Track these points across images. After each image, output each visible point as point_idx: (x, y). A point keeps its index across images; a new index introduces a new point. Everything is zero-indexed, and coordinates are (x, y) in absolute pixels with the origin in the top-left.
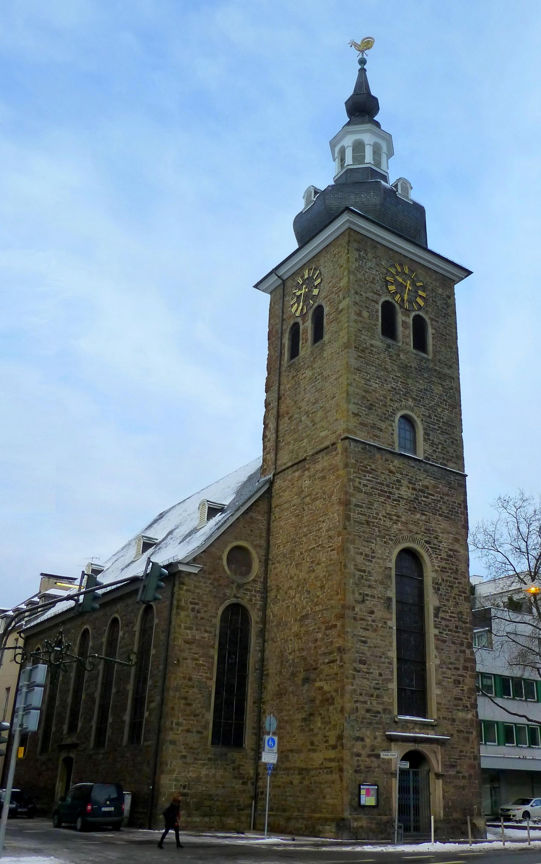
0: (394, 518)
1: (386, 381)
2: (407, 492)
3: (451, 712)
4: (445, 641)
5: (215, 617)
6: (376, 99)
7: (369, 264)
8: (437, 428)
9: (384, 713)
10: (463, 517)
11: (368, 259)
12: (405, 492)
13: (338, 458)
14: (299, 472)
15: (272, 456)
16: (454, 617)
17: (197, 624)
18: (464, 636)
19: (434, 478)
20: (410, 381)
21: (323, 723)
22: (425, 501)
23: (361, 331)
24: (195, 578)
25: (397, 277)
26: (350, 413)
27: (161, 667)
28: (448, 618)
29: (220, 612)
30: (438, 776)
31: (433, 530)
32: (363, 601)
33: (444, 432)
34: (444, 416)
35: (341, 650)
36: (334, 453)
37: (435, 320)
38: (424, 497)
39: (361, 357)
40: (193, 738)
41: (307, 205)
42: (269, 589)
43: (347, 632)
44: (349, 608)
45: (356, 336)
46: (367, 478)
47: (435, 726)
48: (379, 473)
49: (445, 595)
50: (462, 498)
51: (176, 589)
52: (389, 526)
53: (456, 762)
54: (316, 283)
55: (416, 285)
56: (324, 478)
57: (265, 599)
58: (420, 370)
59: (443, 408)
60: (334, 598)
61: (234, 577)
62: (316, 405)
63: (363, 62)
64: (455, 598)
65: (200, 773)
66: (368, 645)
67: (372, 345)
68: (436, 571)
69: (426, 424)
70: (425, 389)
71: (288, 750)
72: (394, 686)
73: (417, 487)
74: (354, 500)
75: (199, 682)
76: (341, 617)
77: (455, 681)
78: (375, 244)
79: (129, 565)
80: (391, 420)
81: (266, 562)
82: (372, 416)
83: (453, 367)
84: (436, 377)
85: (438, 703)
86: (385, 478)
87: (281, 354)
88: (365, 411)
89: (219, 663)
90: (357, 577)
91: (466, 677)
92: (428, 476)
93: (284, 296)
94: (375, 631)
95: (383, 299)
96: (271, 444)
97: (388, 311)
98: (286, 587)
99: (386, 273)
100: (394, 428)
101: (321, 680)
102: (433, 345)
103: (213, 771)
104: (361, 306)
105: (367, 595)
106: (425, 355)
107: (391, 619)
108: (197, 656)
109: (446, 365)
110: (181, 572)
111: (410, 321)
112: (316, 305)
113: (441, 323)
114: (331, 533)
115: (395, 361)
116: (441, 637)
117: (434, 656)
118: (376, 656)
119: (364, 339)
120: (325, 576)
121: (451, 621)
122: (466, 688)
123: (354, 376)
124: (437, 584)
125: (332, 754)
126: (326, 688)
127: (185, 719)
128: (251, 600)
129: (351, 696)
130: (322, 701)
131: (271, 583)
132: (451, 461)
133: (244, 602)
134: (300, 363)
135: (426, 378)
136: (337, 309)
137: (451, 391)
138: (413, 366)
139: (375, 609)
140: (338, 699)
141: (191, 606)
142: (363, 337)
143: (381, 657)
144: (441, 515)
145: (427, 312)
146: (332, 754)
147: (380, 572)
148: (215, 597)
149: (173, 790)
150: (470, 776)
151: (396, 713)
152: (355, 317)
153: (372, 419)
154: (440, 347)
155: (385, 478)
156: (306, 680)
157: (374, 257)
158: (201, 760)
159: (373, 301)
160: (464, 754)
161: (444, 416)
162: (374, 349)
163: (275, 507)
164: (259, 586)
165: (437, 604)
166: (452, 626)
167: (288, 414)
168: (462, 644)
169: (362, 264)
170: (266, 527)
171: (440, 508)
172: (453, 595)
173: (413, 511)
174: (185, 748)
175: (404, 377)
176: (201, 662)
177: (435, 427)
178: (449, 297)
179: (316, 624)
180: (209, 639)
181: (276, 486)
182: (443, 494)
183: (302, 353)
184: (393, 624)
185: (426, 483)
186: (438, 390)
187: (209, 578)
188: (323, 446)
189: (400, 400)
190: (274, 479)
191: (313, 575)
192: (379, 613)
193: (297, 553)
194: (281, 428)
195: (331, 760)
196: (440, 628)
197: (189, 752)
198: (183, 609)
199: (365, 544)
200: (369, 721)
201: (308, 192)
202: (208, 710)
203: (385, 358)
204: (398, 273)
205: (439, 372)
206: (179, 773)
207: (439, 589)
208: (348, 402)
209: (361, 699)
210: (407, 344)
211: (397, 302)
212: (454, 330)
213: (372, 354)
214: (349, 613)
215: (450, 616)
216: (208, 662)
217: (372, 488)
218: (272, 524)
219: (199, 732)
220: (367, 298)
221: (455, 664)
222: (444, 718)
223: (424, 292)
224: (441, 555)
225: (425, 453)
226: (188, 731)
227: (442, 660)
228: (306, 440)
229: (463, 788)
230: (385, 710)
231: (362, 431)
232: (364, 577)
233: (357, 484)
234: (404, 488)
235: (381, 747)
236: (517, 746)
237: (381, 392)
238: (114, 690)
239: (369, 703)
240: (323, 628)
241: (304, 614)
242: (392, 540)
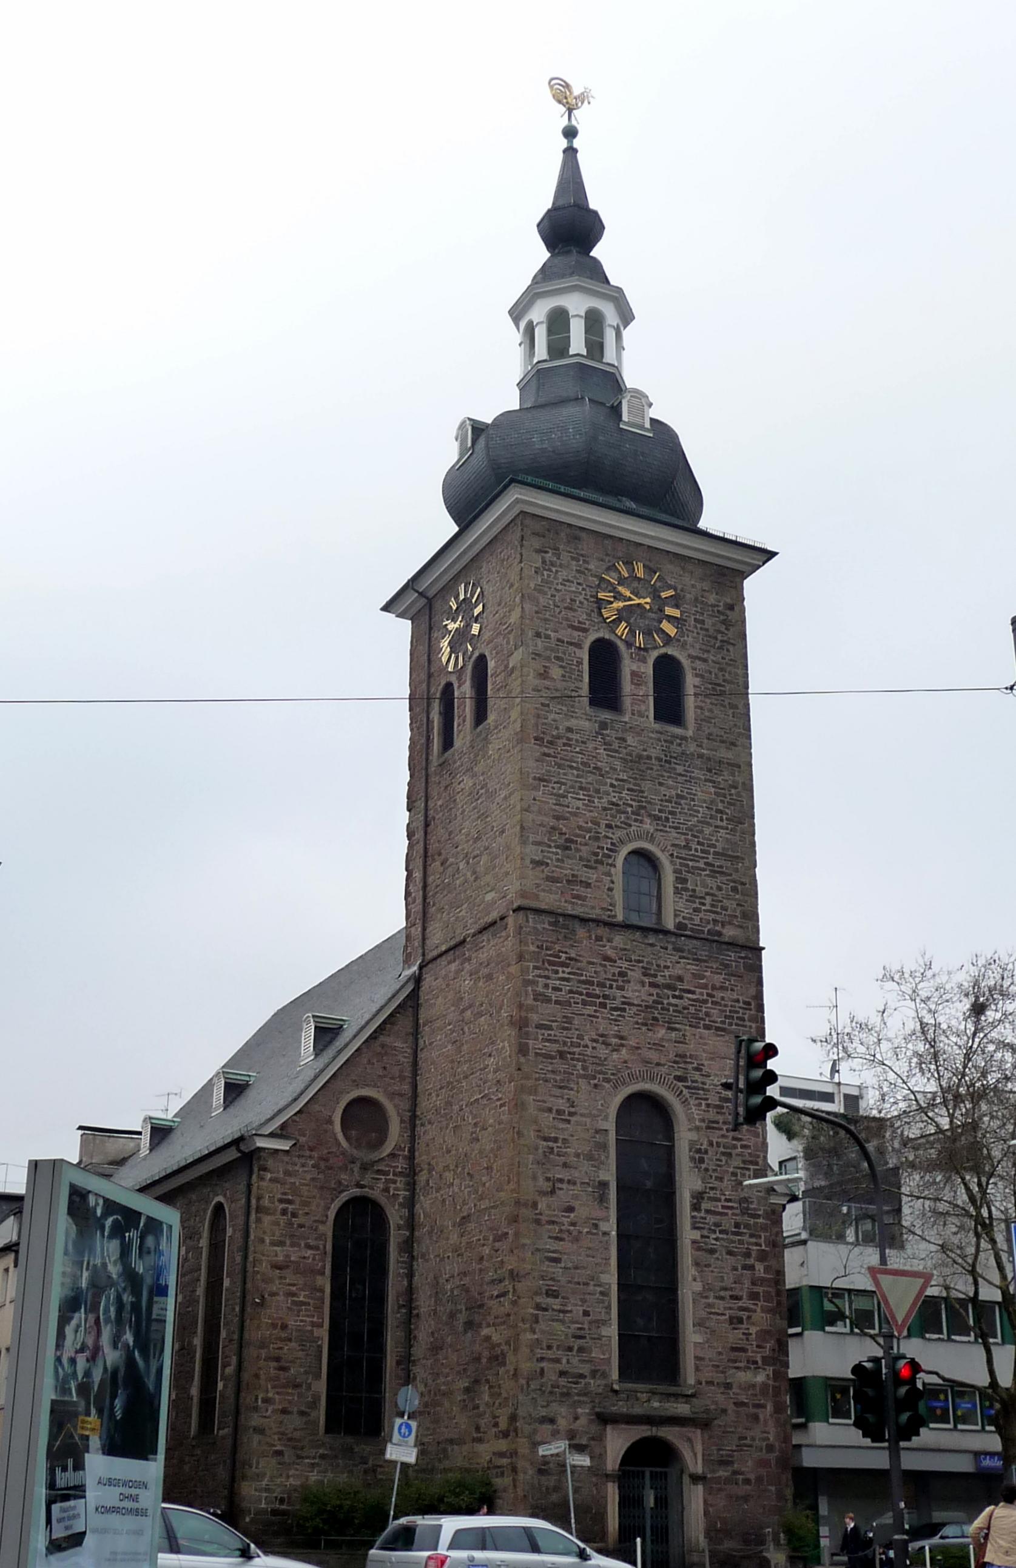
0: (614, 1041)
1: (598, 791)
2: (639, 991)
3: (723, 1372)
4: (712, 1251)
5: (323, 1223)
6: (595, 214)
7: (563, 574)
8: (703, 866)
9: (594, 1377)
10: (754, 1025)
11: (561, 566)
12: (637, 992)
13: (509, 943)
14: (457, 963)
15: (417, 931)
16: (731, 1208)
17: (292, 1236)
18: (753, 1240)
19: (694, 960)
20: (646, 785)
21: (491, 1395)
22: (676, 1006)
23: (548, 705)
24: (286, 1159)
25: (620, 588)
26: (528, 862)
27: (237, 1309)
28: (720, 1210)
29: (332, 1214)
30: (696, 1479)
31: (691, 1056)
32: (553, 1192)
33: (718, 872)
34: (717, 841)
35: (514, 1276)
36: (504, 934)
37: (700, 659)
38: (674, 997)
39: (548, 755)
40: (294, 1422)
41: (461, 456)
42: (418, 1169)
43: (524, 1245)
44: (526, 1205)
45: (538, 716)
46: (561, 975)
47: (693, 1396)
48: (583, 965)
49: (714, 1170)
50: (752, 991)
51: (254, 1177)
52: (603, 1056)
53: (732, 1456)
54: (477, 611)
55: (659, 597)
56: (489, 977)
57: (412, 1186)
58: (669, 762)
59: (716, 827)
60: (506, 1187)
62: (479, 844)
63: (570, 133)
64: (734, 1174)
65: (307, 1478)
66: (563, 1265)
67: (569, 730)
68: (698, 1129)
69: (678, 861)
70: (677, 795)
71: (447, 1440)
72: (612, 1331)
73: (660, 980)
74: (534, 1018)
75: (297, 1331)
76: (514, 1219)
77: (731, 1318)
78: (576, 533)
80: (608, 864)
81: (412, 1121)
82: (570, 862)
83: (739, 743)
84: (701, 769)
85: (697, 1358)
86: (595, 972)
87: (429, 740)
88: (557, 854)
90: (540, 1151)
91: (755, 1311)
92: (680, 958)
93: (431, 629)
94: (576, 1240)
95: (592, 637)
96: (417, 907)
97: (604, 658)
98: (440, 1167)
99: (599, 586)
100: (614, 878)
101: (489, 1326)
102: (696, 707)
103: (330, 1475)
104: (548, 659)
105: (561, 1181)
106: (678, 731)
108: (294, 1288)
109: (722, 742)
110: (260, 1149)
112: (476, 654)
113: (713, 661)
114: (501, 1075)
115: (616, 751)
116: (706, 1244)
117: (690, 1278)
118: (579, 1284)
119: (554, 721)
120: (492, 1149)
121: (726, 1214)
122: (753, 1330)
123: (534, 793)
124: (699, 1151)
125: (502, 1445)
126: (496, 1338)
127: (278, 1393)
128: (386, 1190)
129: (532, 1351)
130: (490, 1359)
131: (421, 1158)
132: (730, 923)
133: (375, 1194)
134: (455, 762)
135: (680, 775)
136: (506, 667)
137: (733, 791)
138: (653, 755)
139: (576, 1204)
140: (510, 1358)
142: (552, 716)
143: (587, 1284)
144: (707, 1027)
145: (684, 646)
146: (502, 1445)
147: (585, 1140)
148: (322, 1188)
149: (263, 1506)
150: (759, 1479)
151: (615, 1375)
152: (537, 682)
153: (571, 867)
154: (711, 711)
155: (595, 972)
156: (469, 1325)
157: (573, 558)
158: (307, 1458)
159: (571, 644)
160: (748, 1442)
161: (717, 841)
162: (574, 736)
163: (425, 1025)
164: (401, 1164)
165: (698, 1186)
166: (728, 1223)
167: (440, 854)
168: (747, 1255)
169: (549, 576)
170: (411, 1060)
171: (707, 1014)
172: (731, 1170)
173: (652, 1025)
174: (279, 1439)
175: (635, 779)
176: (301, 1299)
177: (697, 864)
178: (731, 608)
179: (481, 1231)
180: (314, 1259)
181: (425, 985)
182: (714, 988)
183: (458, 743)
184: (611, 1226)
185: (678, 971)
188: (489, 919)
189: (626, 824)
190: (420, 974)
191: (477, 1146)
192: (585, 1209)
193: (456, 1108)
194: (430, 879)
195: (502, 1455)
196: (703, 1228)
197: (285, 1446)
198: (266, 1211)
199: (558, 1092)
200: (565, 1390)
201: (462, 426)
202: (318, 1376)
203: (596, 749)
204: (622, 581)
205: (709, 759)
206: (272, 1479)
207: (702, 1160)
208: (524, 842)
209: (550, 1354)
210: (641, 715)
211: (620, 638)
212: (740, 672)
213: (570, 746)
214: (525, 1212)
215: (723, 1207)
216: (312, 1298)
217: (571, 992)
218: (422, 1055)
219: (302, 1413)
220: (559, 640)
221: (731, 1289)
222: (710, 1383)
223: (677, 606)
224: (707, 1099)
225: (676, 916)
226: (284, 1411)
228: (465, 906)
229: (746, 1498)
230: (594, 1373)
231: (550, 892)
232: (556, 1150)
233: (540, 989)
234: (632, 986)
235: (587, 1433)
236: (955, 1428)
237: (588, 814)
239: (564, 1361)
240: (491, 1238)
241: (465, 1214)
242: (608, 1081)
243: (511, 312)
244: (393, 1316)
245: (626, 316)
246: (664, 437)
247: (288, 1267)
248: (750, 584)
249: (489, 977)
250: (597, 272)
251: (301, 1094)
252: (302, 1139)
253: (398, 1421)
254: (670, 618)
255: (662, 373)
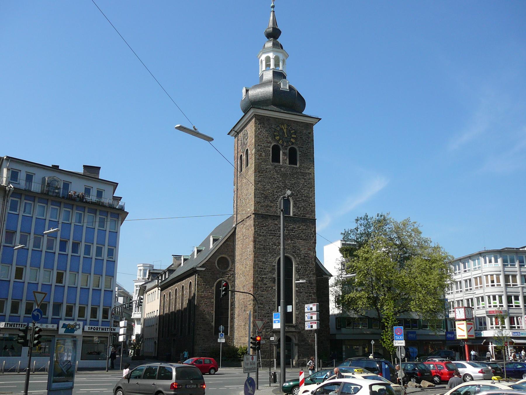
4: (301, 293)
30: (296, 345)
61: (221, 270)
67: (267, 169)
95: (273, 144)
107: (275, 286)
111: (287, 151)
114: (250, 253)
145: (297, 145)
153: (267, 203)
178: (310, 133)
186: (302, 181)
223: (295, 134)
226: (204, 330)
227: (299, 300)
248: (315, 127)
249: (248, 229)
254: (293, 138)
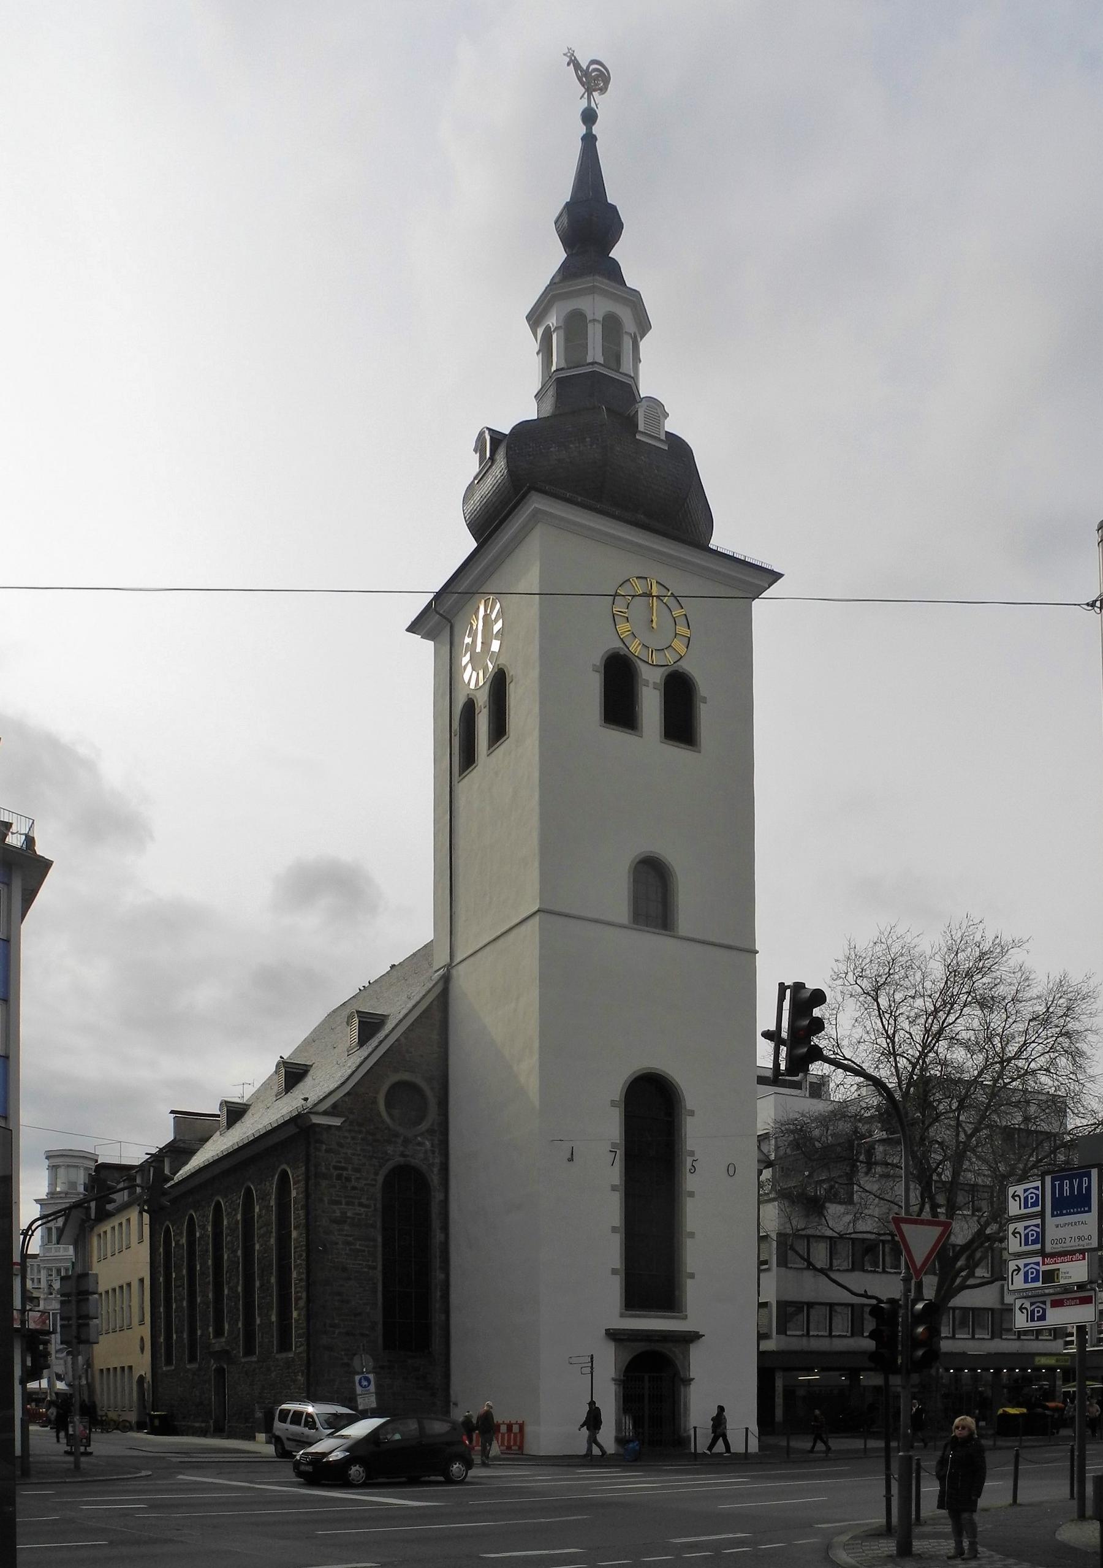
6: (613, 209)
29: (380, 1179)
63: (589, 117)
79: (596, 921)
89: (384, 1245)
141: (335, 1173)
187: (360, 1132)
238: (257, 1284)
243: (529, 318)
244: (437, 1263)
245: (644, 326)
246: (679, 452)
247: (345, 1222)
250: (614, 272)
251: (347, 1079)
252: (351, 1117)
253: (357, 1378)
255: (679, 385)
